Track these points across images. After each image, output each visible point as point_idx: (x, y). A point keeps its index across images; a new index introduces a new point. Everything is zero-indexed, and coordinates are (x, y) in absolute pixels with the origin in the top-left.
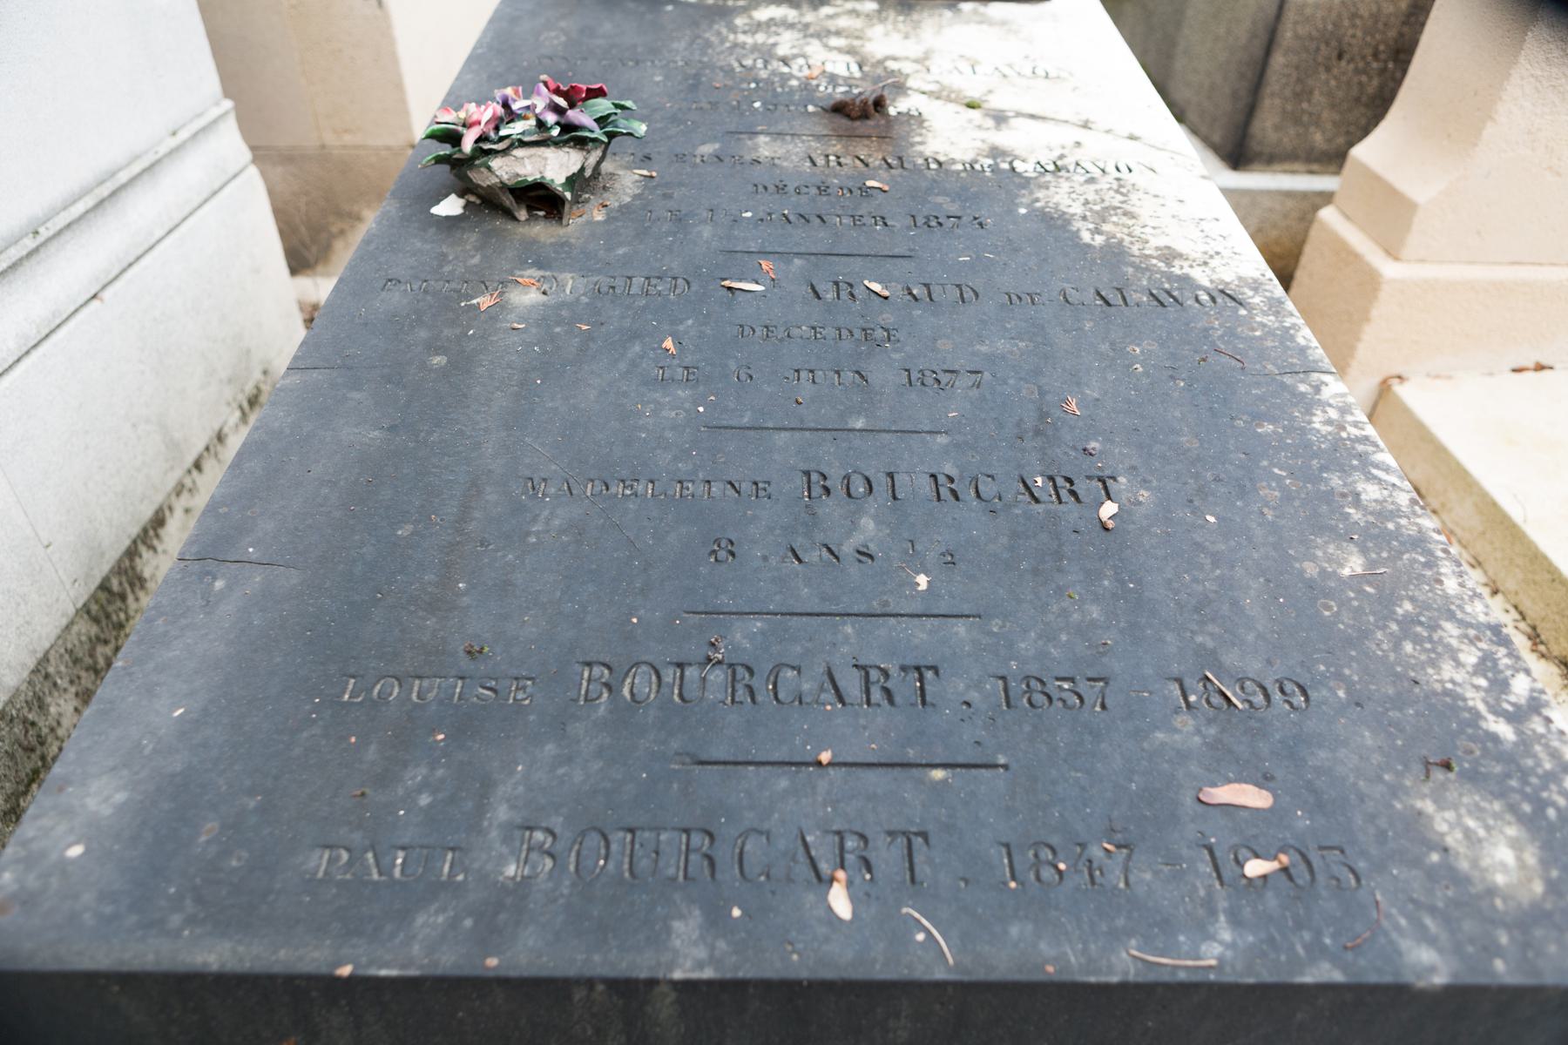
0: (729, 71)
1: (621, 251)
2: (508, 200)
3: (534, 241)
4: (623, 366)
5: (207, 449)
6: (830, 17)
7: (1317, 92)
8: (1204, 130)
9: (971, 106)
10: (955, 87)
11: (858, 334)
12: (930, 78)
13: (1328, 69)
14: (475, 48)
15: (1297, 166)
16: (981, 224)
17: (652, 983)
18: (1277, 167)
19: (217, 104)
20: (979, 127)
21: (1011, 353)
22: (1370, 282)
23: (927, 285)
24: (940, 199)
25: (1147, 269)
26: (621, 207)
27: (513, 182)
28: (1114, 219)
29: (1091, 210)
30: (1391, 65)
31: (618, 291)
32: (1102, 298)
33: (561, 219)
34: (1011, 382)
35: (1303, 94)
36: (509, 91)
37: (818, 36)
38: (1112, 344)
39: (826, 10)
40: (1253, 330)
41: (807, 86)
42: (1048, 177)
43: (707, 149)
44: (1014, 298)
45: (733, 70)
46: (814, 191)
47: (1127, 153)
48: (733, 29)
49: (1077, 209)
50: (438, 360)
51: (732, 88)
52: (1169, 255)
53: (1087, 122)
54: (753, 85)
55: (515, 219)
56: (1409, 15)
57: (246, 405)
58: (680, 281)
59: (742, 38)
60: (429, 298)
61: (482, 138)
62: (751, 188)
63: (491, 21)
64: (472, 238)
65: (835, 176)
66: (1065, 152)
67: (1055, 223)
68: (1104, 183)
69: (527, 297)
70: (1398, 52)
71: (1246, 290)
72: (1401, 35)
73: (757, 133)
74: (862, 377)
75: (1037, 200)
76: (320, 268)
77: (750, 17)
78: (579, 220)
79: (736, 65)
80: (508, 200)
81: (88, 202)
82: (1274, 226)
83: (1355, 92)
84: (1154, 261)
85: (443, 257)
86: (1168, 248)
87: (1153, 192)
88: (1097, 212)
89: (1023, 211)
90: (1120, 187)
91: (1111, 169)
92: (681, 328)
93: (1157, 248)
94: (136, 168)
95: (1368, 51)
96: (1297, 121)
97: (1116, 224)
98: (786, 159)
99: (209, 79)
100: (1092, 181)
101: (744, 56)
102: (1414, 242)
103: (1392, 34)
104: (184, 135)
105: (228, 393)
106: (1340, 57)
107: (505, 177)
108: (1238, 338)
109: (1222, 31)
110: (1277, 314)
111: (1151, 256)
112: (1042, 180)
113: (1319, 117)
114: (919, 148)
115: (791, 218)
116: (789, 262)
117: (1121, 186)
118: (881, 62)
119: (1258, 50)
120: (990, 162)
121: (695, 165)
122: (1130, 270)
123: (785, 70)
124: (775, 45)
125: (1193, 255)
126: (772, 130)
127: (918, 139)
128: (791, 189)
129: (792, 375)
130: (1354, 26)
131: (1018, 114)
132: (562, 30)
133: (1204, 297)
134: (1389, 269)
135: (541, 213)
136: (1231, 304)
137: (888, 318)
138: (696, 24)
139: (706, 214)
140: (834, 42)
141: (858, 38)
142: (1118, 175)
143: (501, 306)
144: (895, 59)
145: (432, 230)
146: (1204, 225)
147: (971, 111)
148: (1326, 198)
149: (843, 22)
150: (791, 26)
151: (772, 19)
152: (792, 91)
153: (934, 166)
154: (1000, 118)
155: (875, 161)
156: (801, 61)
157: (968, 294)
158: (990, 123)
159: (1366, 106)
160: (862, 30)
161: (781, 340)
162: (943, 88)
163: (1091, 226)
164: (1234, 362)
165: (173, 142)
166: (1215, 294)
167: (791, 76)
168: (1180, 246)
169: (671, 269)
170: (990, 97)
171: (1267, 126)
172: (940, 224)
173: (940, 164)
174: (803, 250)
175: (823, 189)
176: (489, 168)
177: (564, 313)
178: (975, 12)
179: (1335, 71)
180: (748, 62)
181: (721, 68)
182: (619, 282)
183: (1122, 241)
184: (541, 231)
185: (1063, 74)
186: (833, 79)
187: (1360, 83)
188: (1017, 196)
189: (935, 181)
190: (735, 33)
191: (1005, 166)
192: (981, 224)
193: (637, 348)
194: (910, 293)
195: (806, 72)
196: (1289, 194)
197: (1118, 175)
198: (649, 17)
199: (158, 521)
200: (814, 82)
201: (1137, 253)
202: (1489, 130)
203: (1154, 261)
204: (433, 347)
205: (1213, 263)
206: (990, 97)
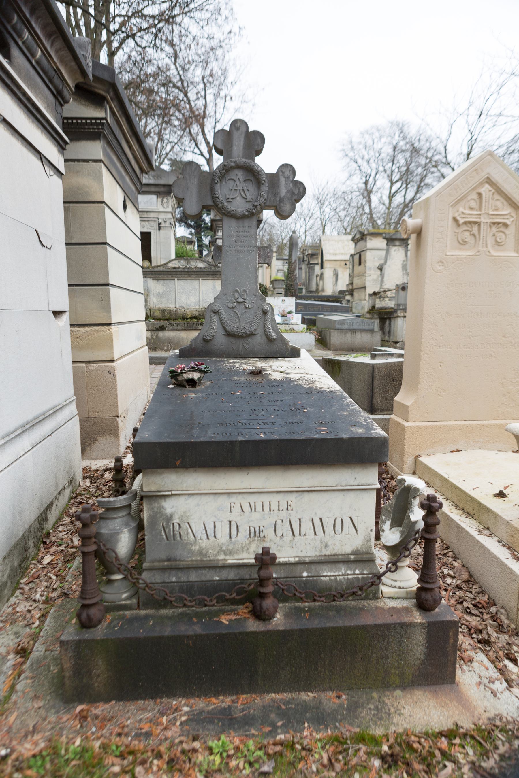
2: (185, 383)
13: (391, 384)
17: (236, 441)
22: (403, 427)
52: (322, 388)
81: (29, 426)
94: (60, 407)
96: (386, 399)
99: (72, 392)
102: (411, 417)
104: (67, 402)
106: (393, 381)
119: (370, 381)
134: (406, 424)
154: (288, 374)
199: (51, 504)
202: (419, 386)
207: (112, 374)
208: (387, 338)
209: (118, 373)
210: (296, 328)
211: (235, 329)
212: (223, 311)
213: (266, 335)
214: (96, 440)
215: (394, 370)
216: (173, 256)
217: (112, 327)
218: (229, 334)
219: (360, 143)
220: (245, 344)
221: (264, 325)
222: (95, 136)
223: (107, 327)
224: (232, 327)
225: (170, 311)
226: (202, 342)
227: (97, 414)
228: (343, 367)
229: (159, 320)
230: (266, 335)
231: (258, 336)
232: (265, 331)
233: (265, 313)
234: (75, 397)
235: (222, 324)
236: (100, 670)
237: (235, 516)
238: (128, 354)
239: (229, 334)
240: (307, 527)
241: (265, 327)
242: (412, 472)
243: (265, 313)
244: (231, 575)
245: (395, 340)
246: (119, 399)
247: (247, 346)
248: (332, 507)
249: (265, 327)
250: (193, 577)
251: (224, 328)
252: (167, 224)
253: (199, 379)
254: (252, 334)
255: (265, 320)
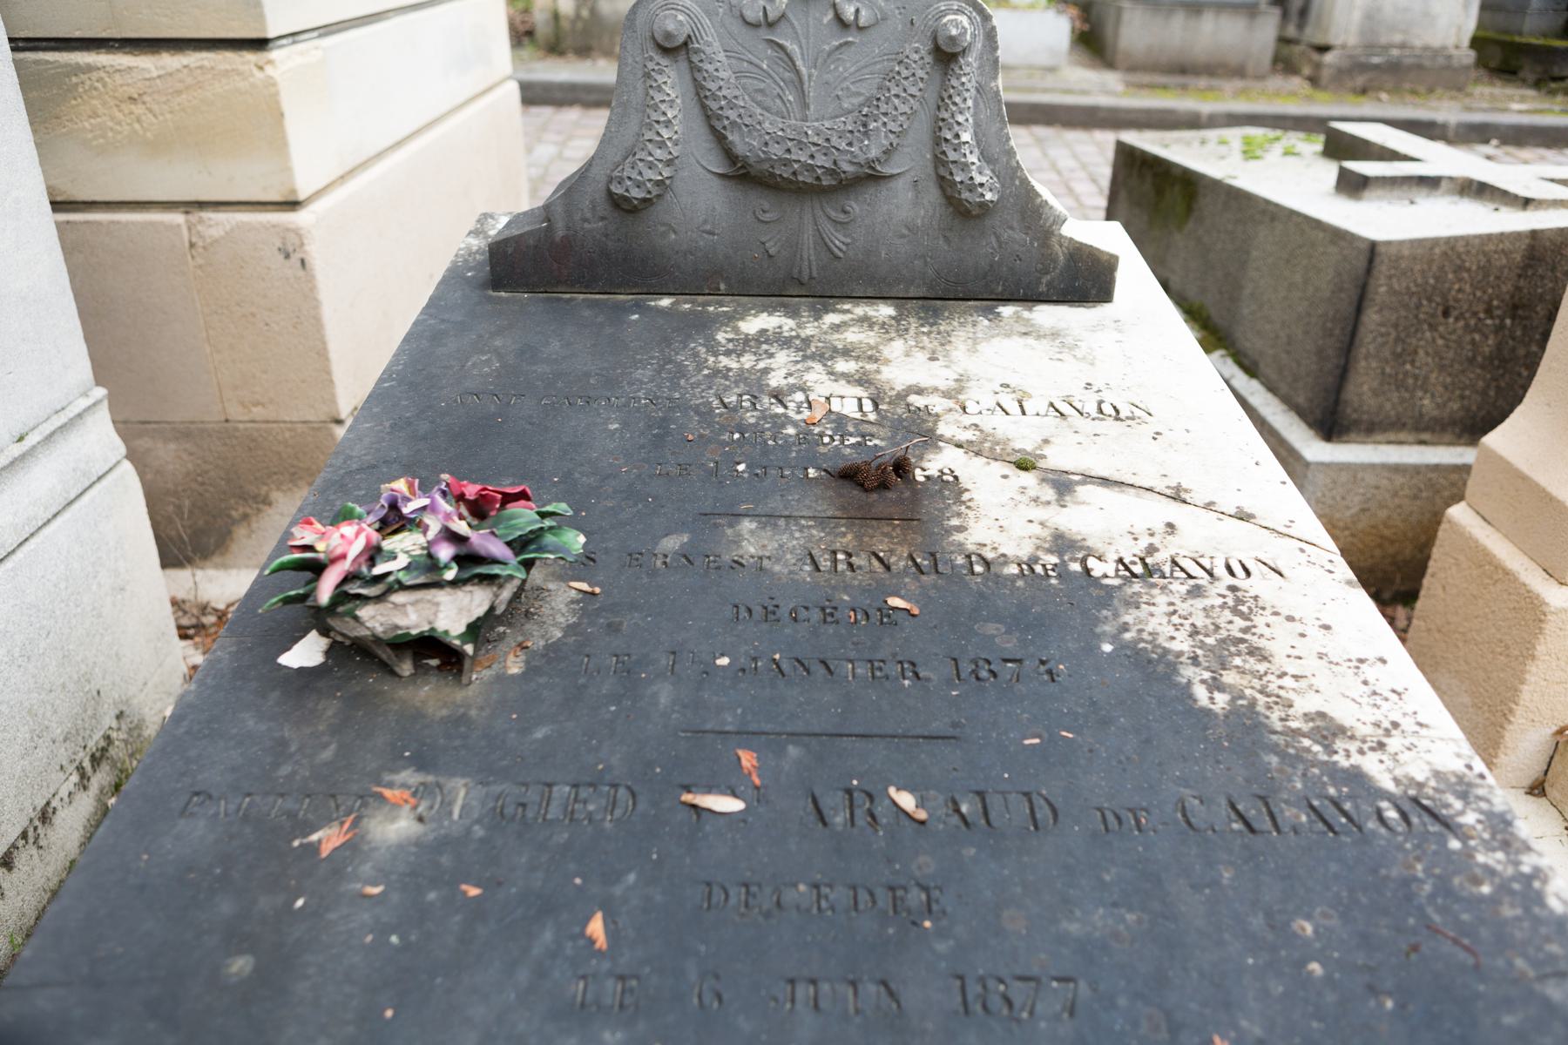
0: (705, 413)
1: (539, 734)
3: (418, 715)
4: (523, 976)
5: (24, 835)
6: (836, 328)
7: (1421, 353)
8: (1284, 388)
9: (1023, 466)
10: (1000, 434)
11: (884, 899)
12: (967, 420)
13: (1432, 327)
14: (381, 380)
15: (1402, 436)
16: (1050, 672)
18: (1379, 437)
19: (85, 394)
20: (1036, 500)
21: (1116, 935)
22: (1533, 612)
23: (981, 794)
24: (991, 628)
25: (1298, 758)
26: (547, 647)
27: (391, 635)
28: (1237, 661)
29: (1202, 645)
30: (1508, 322)
31: (530, 814)
32: (1241, 817)
33: (460, 671)
34: (1122, 1001)
35: (1404, 355)
36: (401, 485)
37: (820, 357)
38: (1269, 915)
39: (831, 318)
40: (1477, 882)
41: (806, 435)
42: (1137, 587)
43: (672, 543)
44: (1111, 818)
45: (712, 410)
46: (816, 615)
47: (1241, 543)
48: (713, 349)
49: (1182, 644)
50: (240, 965)
51: (709, 441)
52: (1328, 730)
53: (1178, 488)
54: (736, 436)
55: (393, 673)
56: (1526, 267)
57: (87, 764)
58: (622, 792)
59: (724, 361)
60: (248, 830)
61: (348, 578)
62: (729, 612)
63: (406, 340)
64: (330, 708)
65: (847, 588)
66: (1156, 541)
67: (1152, 668)
68: (1216, 594)
69: (395, 828)
70: (1515, 307)
71: (1451, 799)
72: (1518, 289)
73: (740, 515)
74: (891, 993)
75: (1125, 628)
76: (216, 559)
77: (736, 330)
78: (487, 673)
79: (716, 403)
80: (385, 654)
82: (1382, 506)
83: (1467, 351)
84: (1306, 742)
85: (280, 749)
86: (1322, 715)
87: (1285, 612)
88: (1211, 649)
89: (1107, 648)
90: (1239, 604)
91: (1220, 571)
92: (618, 891)
93: (1307, 717)
95: (1481, 307)
96: (1400, 385)
97: (1241, 671)
98: (778, 560)
99: (80, 365)
100: (1196, 592)
101: (727, 389)
103: (1506, 288)
105: (63, 755)
106: (1446, 314)
107: (379, 629)
108: (1459, 899)
109: (1298, 278)
110: (1506, 845)
111: (1297, 733)
112: (1129, 591)
113: (1426, 378)
114: (958, 537)
115: (784, 666)
116: (780, 751)
117: (1239, 601)
118: (902, 396)
119: (1347, 309)
120: (1054, 559)
121: (653, 573)
122: (1274, 760)
123: (780, 410)
124: (766, 371)
125: (1363, 730)
126: (759, 511)
127: (955, 522)
128: (784, 612)
129: (783, 990)
130: (1460, 280)
131: (1088, 478)
132: (496, 351)
133: (1392, 814)
135: (434, 662)
136: (1434, 828)
137: (926, 864)
138: (667, 341)
139: (665, 661)
140: (842, 366)
141: (871, 359)
142: (1230, 581)
143: (353, 848)
144: (920, 391)
145: (275, 695)
146: (1368, 671)
147: (1022, 473)
148: (1453, 483)
149: (853, 336)
150: (786, 343)
151: (763, 331)
152: (786, 447)
153: (978, 569)
154: (1063, 485)
155: (899, 563)
156: (799, 396)
157: (1043, 813)
158: (1049, 493)
159: (1482, 367)
160: (875, 347)
161: (768, 915)
162: (985, 437)
163: (1207, 675)
164: (1462, 955)
165: (17, 450)
166: (1407, 806)
167: (788, 420)
168: (1343, 713)
169: (608, 768)
170: (1047, 451)
171: (1363, 389)
172: (994, 674)
173: (987, 564)
174: (799, 726)
175: (829, 613)
176: (356, 618)
177: (445, 860)
178: (1018, 318)
179: (1441, 329)
180: (732, 399)
181: (697, 410)
182: (533, 795)
183: (1253, 703)
184: (428, 695)
185: (1138, 413)
186: (840, 421)
187: (1473, 342)
188: (1098, 621)
189: (981, 595)
190: (716, 355)
191: (1076, 567)
192: (1050, 672)
193: (548, 936)
194: (958, 811)
195: (806, 414)
196: (1397, 469)
197: (1230, 581)
198: (608, 330)
200: (817, 430)
201: (1278, 726)
203: (1306, 742)
204: (236, 939)
205: (1394, 743)
206: (1047, 451)
207: (295, 258)
208: (1291, 31)
209: (315, 252)
211: (776, 151)
212: (712, 44)
213: (945, 184)
214: (267, 502)
215: (1459, 269)
217: (274, 54)
218: (744, 174)
220: (827, 227)
221: (938, 125)
223: (250, 57)
224: (767, 132)
226: (604, 208)
227: (258, 413)
228: (1205, 202)
230: (945, 184)
231: (900, 184)
232: (939, 161)
233: (946, 56)
234: (101, 392)
235: (709, 117)
238: (380, 155)
239: (744, 174)
241: (938, 141)
242: (1527, 782)
243: (946, 56)
245: (1320, 40)
246: (334, 356)
247: (838, 240)
249: (938, 141)
251: (720, 138)
253: (475, 630)
254: (870, 177)
255: (942, 102)
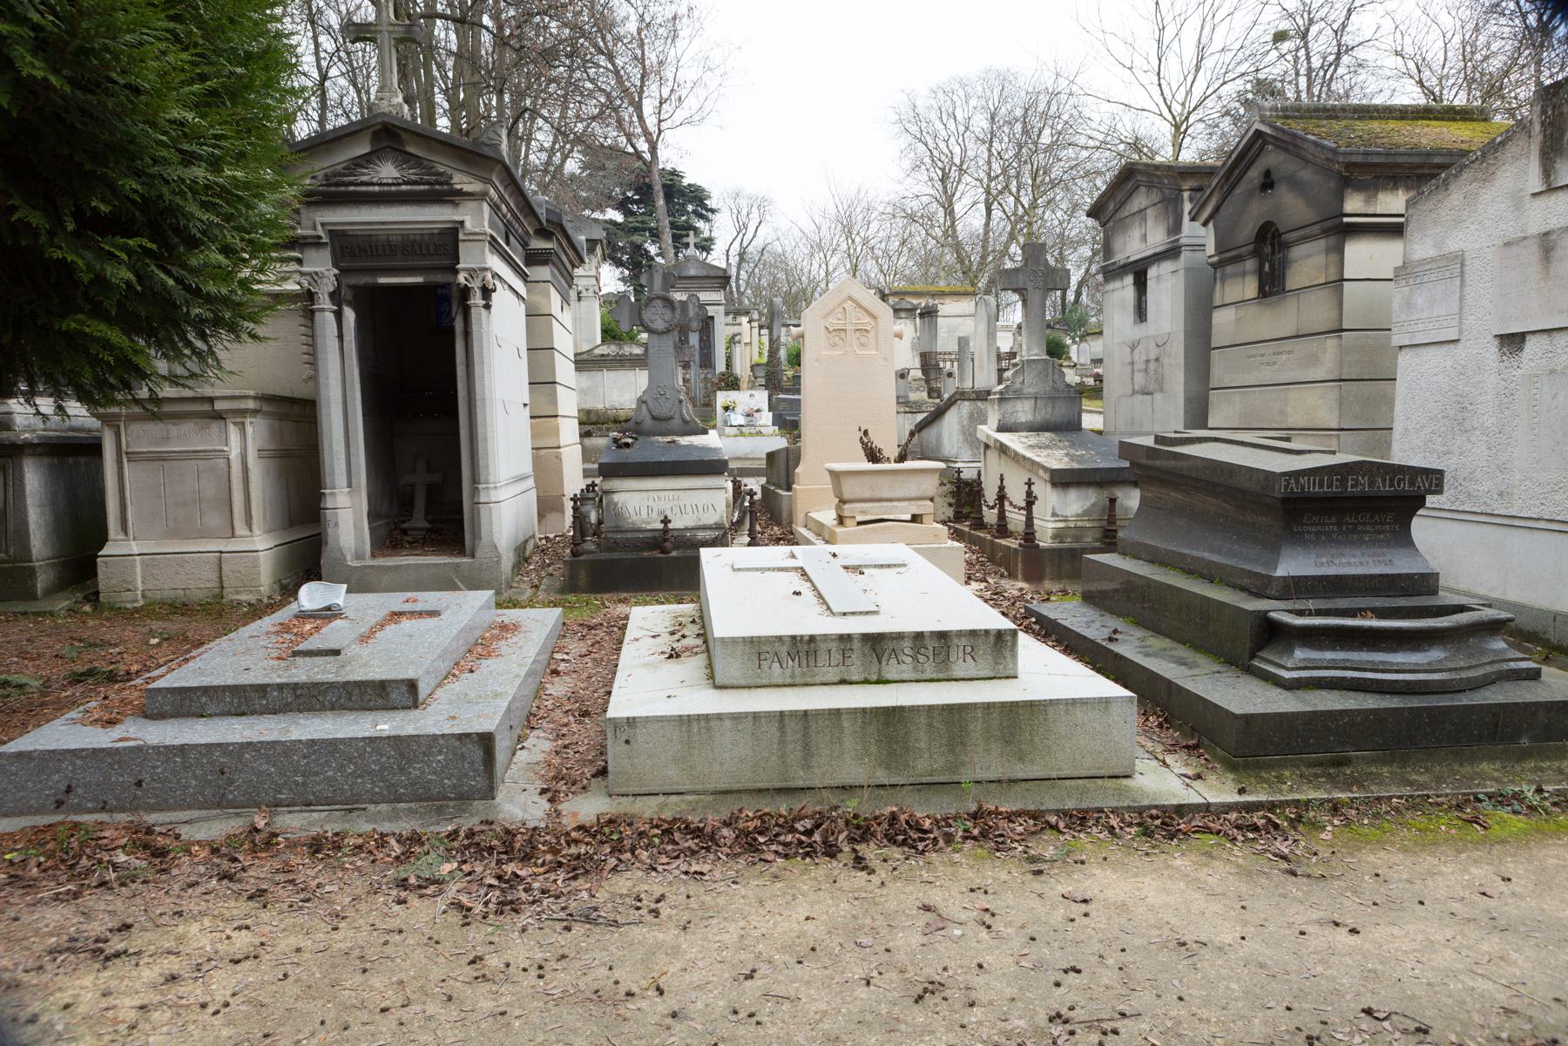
210: (764, 430)
216: (599, 341)
218: (654, 418)
219: (930, 108)
222: (544, 263)
225: (597, 412)
229: (591, 423)
236: (583, 576)
237: (651, 503)
239: (654, 418)
240: (689, 509)
244: (649, 535)
248: (702, 498)
250: (629, 535)
252: (590, 293)
